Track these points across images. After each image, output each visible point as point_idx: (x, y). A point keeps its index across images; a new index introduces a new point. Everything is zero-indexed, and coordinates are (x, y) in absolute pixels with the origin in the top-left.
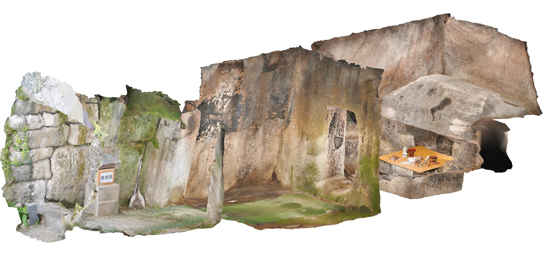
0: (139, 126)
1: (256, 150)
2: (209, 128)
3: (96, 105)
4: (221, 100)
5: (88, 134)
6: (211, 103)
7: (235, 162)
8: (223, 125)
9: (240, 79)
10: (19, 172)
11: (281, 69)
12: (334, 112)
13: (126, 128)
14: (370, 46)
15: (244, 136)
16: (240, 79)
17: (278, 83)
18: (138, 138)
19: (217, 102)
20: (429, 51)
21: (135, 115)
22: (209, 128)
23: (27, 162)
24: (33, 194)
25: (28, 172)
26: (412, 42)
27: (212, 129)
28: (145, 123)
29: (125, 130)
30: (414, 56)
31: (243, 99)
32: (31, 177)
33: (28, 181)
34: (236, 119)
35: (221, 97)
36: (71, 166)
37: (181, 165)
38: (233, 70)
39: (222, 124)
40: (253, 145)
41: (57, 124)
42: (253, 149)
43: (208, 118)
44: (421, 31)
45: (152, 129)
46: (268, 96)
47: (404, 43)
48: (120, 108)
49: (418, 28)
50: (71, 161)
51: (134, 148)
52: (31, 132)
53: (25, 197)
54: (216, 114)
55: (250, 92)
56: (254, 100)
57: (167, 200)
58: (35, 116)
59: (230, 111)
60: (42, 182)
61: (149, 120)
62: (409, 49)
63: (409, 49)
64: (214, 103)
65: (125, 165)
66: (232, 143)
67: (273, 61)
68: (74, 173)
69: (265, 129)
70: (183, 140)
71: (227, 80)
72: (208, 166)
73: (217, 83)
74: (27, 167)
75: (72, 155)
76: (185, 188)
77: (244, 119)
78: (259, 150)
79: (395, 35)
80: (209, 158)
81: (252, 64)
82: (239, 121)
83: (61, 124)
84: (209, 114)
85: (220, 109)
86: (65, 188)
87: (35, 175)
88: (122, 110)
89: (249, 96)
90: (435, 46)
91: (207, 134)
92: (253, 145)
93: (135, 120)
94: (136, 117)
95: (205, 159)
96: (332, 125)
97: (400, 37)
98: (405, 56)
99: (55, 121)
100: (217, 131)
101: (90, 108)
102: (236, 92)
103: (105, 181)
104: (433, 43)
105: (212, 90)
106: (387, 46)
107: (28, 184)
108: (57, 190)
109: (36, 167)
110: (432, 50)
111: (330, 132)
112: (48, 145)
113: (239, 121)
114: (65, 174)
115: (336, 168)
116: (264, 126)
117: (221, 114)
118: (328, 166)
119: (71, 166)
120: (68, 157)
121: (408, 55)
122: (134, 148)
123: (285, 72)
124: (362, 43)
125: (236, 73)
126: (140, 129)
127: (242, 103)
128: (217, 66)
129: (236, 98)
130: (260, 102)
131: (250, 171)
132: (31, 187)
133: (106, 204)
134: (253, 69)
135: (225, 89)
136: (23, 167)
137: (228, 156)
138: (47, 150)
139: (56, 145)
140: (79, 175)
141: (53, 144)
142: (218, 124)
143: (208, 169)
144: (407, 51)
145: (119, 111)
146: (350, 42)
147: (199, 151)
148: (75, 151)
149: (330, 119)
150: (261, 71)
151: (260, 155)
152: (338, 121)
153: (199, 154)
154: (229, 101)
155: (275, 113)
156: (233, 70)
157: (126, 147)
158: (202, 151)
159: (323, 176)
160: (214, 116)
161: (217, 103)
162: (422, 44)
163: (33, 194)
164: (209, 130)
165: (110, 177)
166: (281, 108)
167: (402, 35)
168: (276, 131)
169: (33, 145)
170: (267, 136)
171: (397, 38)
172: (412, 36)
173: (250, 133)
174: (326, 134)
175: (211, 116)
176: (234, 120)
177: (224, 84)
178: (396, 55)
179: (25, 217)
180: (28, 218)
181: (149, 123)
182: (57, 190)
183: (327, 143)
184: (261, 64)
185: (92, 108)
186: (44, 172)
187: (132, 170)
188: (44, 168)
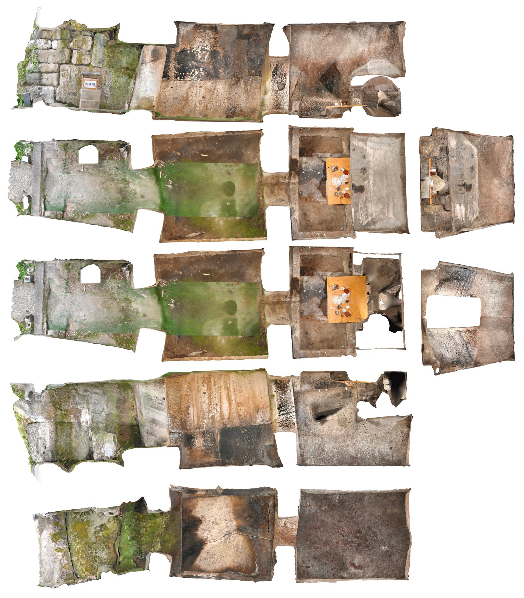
0: (124, 56)
1: (240, 96)
2: (193, 71)
3: (90, 38)
4: (200, 52)
5: (84, 57)
6: (191, 52)
7: (222, 101)
8: (206, 71)
9: (215, 39)
10: (30, 77)
11: (255, 40)
12: (275, 64)
13: (113, 56)
14: (334, 37)
15: (228, 83)
16: (215, 39)
17: (253, 49)
18: (124, 65)
19: (197, 53)
20: (387, 49)
21: (120, 47)
22: (193, 71)
23: (36, 70)
24: (41, 94)
25: (38, 78)
26: (371, 40)
27: (196, 73)
28: (128, 55)
29: (113, 57)
30: (375, 51)
31: (221, 55)
32: (40, 82)
33: (38, 85)
34: (217, 69)
35: (200, 49)
36: (70, 77)
37: (148, 83)
38: (207, 31)
39: (204, 70)
40: (236, 91)
41: (60, 47)
42: (237, 94)
43: (191, 63)
44: (379, 34)
45: (134, 59)
46: (246, 57)
47: (364, 40)
48: (102, 38)
49: (375, 31)
50: (70, 74)
51: (124, 73)
52: (40, 50)
53: (35, 95)
54: (198, 62)
55: (227, 51)
56: (232, 58)
57: (136, 105)
58: (43, 40)
59: (210, 62)
60: (51, 88)
61: (131, 53)
62: (370, 45)
63: (370, 45)
64: (194, 52)
65: (118, 85)
66: (217, 87)
67: (246, 32)
68: (74, 83)
69: (245, 81)
70: (148, 65)
71: (203, 38)
72: (197, 100)
73: (194, 38)
74: (37, 75)
75: (72, 70)
76: (155, 99)
77: (225, 71)
78: (242, 97)
79: (355, 32)
80: (198, 94)
81: (225, 30)
82: (220, 71)
83: (63, 48)
84: (191, 61)
85: (201, 58)
86: (69, 94)
87: (44, 81)
88: (104, 40)
89: (226, 53)
90: (393, 47)
91: (192, 76)
92: (236, 91)
93: (121, 51)
94: (121, 49)
95: (194, 94)
96: (274, 72)
97: (360, 35)
98: (366, 49)
99: (58, 44)
100: (202, 75)
101: (85, 38)
102: (215, 48)
103: (89, 86)
104: (391, 44)
105: (190, 42)
106: (350, 39)
107: (37, 87)
108: (63, 95)
109: (45, 76)
110: (391, 49)
111: (273, 77)
112: (54, 61)
113: (220, 71)
114: (66, 82)
115: (280, 104)
116: (245, 79)
117: (202, 63)
118: (273, 101)
119: (70, 77)
120: (69, 71)
121: (369, 49)
122: (124, 73)
123: (259, 42)
124: (327, 33)
125: (211, 34)
126: (125, 58)
127: (220, 57)
128: (192, 26)
129: (214, 54)
130: (238, 60)
131: (237, 111)
132: (40, 89)
133: (88, 102)
134: (227, 34)
135: (202, 44)
136: (33, 74)
137: (215, 96)
138: (53, 65)
139: (60, 62)
140: (78, 85)
141: (57, 61)
142: (201, 70)
143: (197, 103)
144: (367, 46)
145: (102, 40)
146: (316, 31)
147: (187, 87)
148: (75, 68)
149: (273, 68)
150: (235, 37)
151: (245, 101)
152: (280, 71)
153: (187, 90)
154: (208, 54)
155: (253, 71)
156: (207, 31)
157: (118, 71)
158: (190, 88)
159: (269, 107)
160: (196, 63)
161: (197, 54)
162: (381, 43)
163: (41, 94)
164: (194, 73)
165: (93, 84)
166: (258, 68)
167: (362, 33)
168: (256, 85)
169: (42, 60)
170: (248, 87)
171: (358, 35)
172: (371, 35)
173: (233, 82)
174: (270, 78)
175: (193, 62)
176: (216, 69)
177: (201, 40)
178: (358, 47)
179: (21, 102)
180: (23, 103)
181: (131, 55)
182: (63, 95)
183: (271, 85)
184: (235, 32)
185: (87, 39)
186: (52, 80)
187: (125, 90)
188: (52, 78)
